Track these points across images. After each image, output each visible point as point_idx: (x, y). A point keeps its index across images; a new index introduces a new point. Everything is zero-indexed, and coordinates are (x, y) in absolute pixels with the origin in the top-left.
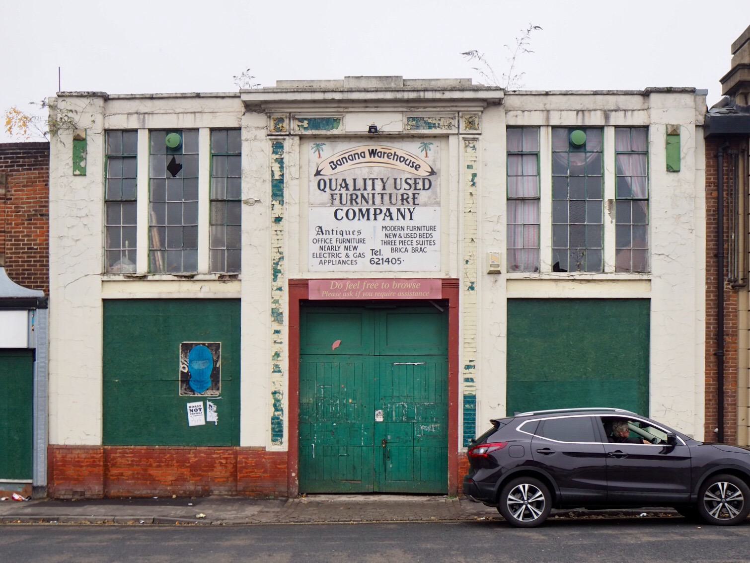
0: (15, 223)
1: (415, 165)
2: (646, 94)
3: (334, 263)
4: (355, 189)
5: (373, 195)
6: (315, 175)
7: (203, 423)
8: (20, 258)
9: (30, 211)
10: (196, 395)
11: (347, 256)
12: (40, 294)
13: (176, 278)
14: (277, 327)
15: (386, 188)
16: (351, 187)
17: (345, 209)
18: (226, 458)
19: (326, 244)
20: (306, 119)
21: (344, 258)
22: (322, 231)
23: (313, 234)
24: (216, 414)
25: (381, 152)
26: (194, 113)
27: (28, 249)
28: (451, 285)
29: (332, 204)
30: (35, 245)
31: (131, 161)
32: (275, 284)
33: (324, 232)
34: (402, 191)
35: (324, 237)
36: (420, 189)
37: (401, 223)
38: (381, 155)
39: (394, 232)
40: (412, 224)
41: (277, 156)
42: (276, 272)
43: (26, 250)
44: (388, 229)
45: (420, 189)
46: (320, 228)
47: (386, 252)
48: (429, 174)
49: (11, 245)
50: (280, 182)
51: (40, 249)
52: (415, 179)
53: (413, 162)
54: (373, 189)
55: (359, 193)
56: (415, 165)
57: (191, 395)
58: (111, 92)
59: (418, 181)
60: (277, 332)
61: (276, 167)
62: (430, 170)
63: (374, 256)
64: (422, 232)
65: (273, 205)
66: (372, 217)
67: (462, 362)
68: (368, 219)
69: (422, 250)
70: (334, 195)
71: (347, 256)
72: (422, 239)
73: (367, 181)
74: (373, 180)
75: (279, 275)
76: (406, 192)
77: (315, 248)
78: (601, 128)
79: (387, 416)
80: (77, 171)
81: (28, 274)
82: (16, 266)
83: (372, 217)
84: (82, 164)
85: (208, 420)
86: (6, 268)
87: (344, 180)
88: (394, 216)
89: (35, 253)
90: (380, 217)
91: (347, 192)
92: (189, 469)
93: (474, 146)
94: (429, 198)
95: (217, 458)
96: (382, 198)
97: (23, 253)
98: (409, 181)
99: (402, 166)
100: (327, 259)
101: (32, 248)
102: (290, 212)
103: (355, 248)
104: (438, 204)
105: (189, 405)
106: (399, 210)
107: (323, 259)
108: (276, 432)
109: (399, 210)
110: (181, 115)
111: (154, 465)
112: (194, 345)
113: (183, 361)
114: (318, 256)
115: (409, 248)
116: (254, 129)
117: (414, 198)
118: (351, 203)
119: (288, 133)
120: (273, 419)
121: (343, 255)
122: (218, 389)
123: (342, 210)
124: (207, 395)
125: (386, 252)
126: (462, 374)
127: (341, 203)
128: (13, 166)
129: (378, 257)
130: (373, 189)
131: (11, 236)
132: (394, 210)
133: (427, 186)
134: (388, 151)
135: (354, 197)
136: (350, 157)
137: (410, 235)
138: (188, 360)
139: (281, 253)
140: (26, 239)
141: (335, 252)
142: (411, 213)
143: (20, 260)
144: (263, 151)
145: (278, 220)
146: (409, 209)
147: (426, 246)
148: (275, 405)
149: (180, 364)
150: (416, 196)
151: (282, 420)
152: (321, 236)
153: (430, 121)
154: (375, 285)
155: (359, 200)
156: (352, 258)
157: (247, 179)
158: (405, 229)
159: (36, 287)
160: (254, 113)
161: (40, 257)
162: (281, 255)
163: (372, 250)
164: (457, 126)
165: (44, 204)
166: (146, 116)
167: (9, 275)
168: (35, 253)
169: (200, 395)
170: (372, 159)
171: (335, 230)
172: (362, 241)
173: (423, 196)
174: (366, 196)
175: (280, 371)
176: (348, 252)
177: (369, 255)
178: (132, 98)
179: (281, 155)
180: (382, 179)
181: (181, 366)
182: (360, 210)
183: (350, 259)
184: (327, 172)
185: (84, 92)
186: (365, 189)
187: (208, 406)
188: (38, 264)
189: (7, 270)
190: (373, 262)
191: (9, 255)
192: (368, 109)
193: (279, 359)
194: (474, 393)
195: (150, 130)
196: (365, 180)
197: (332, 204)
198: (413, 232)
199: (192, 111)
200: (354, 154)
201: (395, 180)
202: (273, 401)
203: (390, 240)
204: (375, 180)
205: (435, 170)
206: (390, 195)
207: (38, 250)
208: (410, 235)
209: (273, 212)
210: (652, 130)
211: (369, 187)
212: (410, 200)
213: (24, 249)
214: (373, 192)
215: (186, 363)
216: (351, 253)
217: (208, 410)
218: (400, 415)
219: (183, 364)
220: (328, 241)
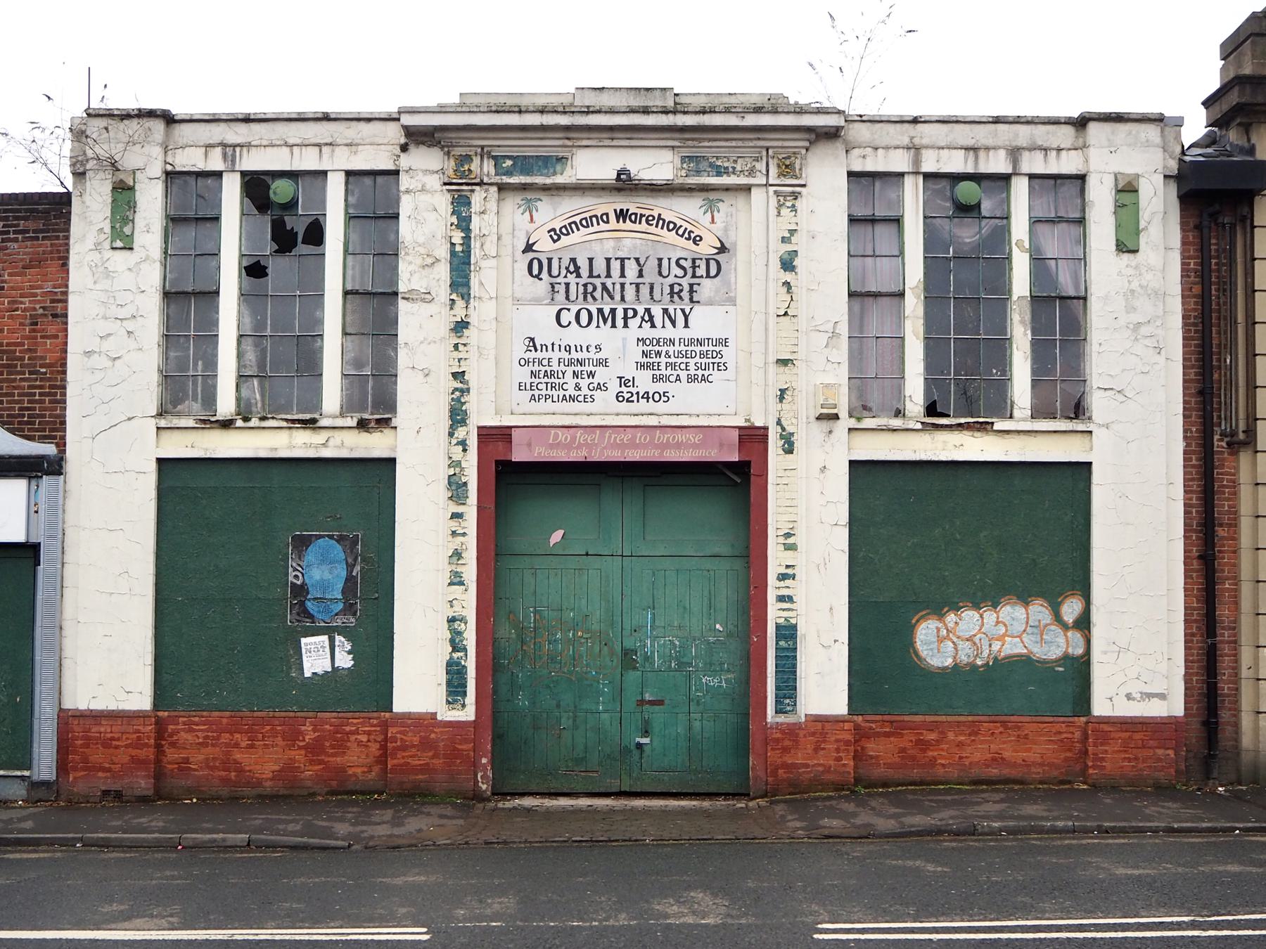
1: (693, 235)
2: (1081, 123)
3: (555, 399)
4: (591, 276)
5: (623, 285)
6: (524, 252)
8: (15, 388)
11: (578, 387)
12: (49, 449)
15: (644, 273)
16: (584, 272)
17: (574, 309)
18: (369, 733)
21: (572, 392)
23: (519, 351)
28: (753, 437)
29: (552, 299)
33: (539, 347)
34: (671, 280)
35: (539, 355)
36: (702, 277)
37: (669, 332)
38: (637, 218)
39: (657, 348)
40: (687, 334)
45: (702, 277)
46: (532, 340)
47: (644, 381)
48: (717, 251)
51: (52, 373)
52: (694, 260)
54: (623, 275)
55: (597, 282)
56: (693, 235)
58: (177, 110)
62: (719, 246)
63: (624, 389)
64: (705, 348)
66: (620, 322)
68: (614, 326)
69: (704, 379)
71: (578, 387)
73: (612, 261)
74: (622, 260)
77: (524, 375)
78: (1005, 179)
83: (620, 322)
84: (127, 230)
87: (573, 260)
88: (658, 320)
89: (41, 380)
91: (578, 280)
94: (717, 291)
96: (638, 291)
98: (682, 262)
99: (671, 237)
100: (544, 392)
101: (37, 372)
102: (481, 313)
103: (592, 375)
104: (732, 301)
105: (304, 640)
106: (665, 311)
107: (536, 393)
109: (665, 311)
111: (243, 744)
113: (294, 565)
114: (528, 387)
115: (683, 375)
116: (420, 174)
117: (691, 291)
118: (585, 298)
123: (569, 310)
125: (644, 381)
126: (773, 588)
127: (567, 298)
129: (631, 389)
130: (623, 275)
132: (657, 311)
134: (647, 213)
141: (557, 381)
143: (16, 391)
146: (683, 310)
147: (711, 371)
148: (452, 641)
149: (290, 570)
152: (532, 355)
154: (626, 437)
155: (598, 294)
156: (585, 391)
159: (43, 439)
163: (621, 378)
164: (765, 172)
165: (59, 297)
170: (621, 225)
172: (603, 363)
173: (707, 288)
174: (610, 287)
176: (579, 380)
177: (614, 387)
178: (214, 120)
180: (637, 260)
181: (291, 573)
182: (600, 311)
183: (582, 393)
186: (609, 276)
194: (793, 621)
196: (608, 260)
197: (552, 299)
198: (690, 348)
200: (591, 217)
201: (660, 260)
205: (727, 245)
209: (452, 312)
211: (616, 270)
212: (685, 295)
215: (300, 569)
216: (584, 383)
219: (295, 570)
220: (545, 362)
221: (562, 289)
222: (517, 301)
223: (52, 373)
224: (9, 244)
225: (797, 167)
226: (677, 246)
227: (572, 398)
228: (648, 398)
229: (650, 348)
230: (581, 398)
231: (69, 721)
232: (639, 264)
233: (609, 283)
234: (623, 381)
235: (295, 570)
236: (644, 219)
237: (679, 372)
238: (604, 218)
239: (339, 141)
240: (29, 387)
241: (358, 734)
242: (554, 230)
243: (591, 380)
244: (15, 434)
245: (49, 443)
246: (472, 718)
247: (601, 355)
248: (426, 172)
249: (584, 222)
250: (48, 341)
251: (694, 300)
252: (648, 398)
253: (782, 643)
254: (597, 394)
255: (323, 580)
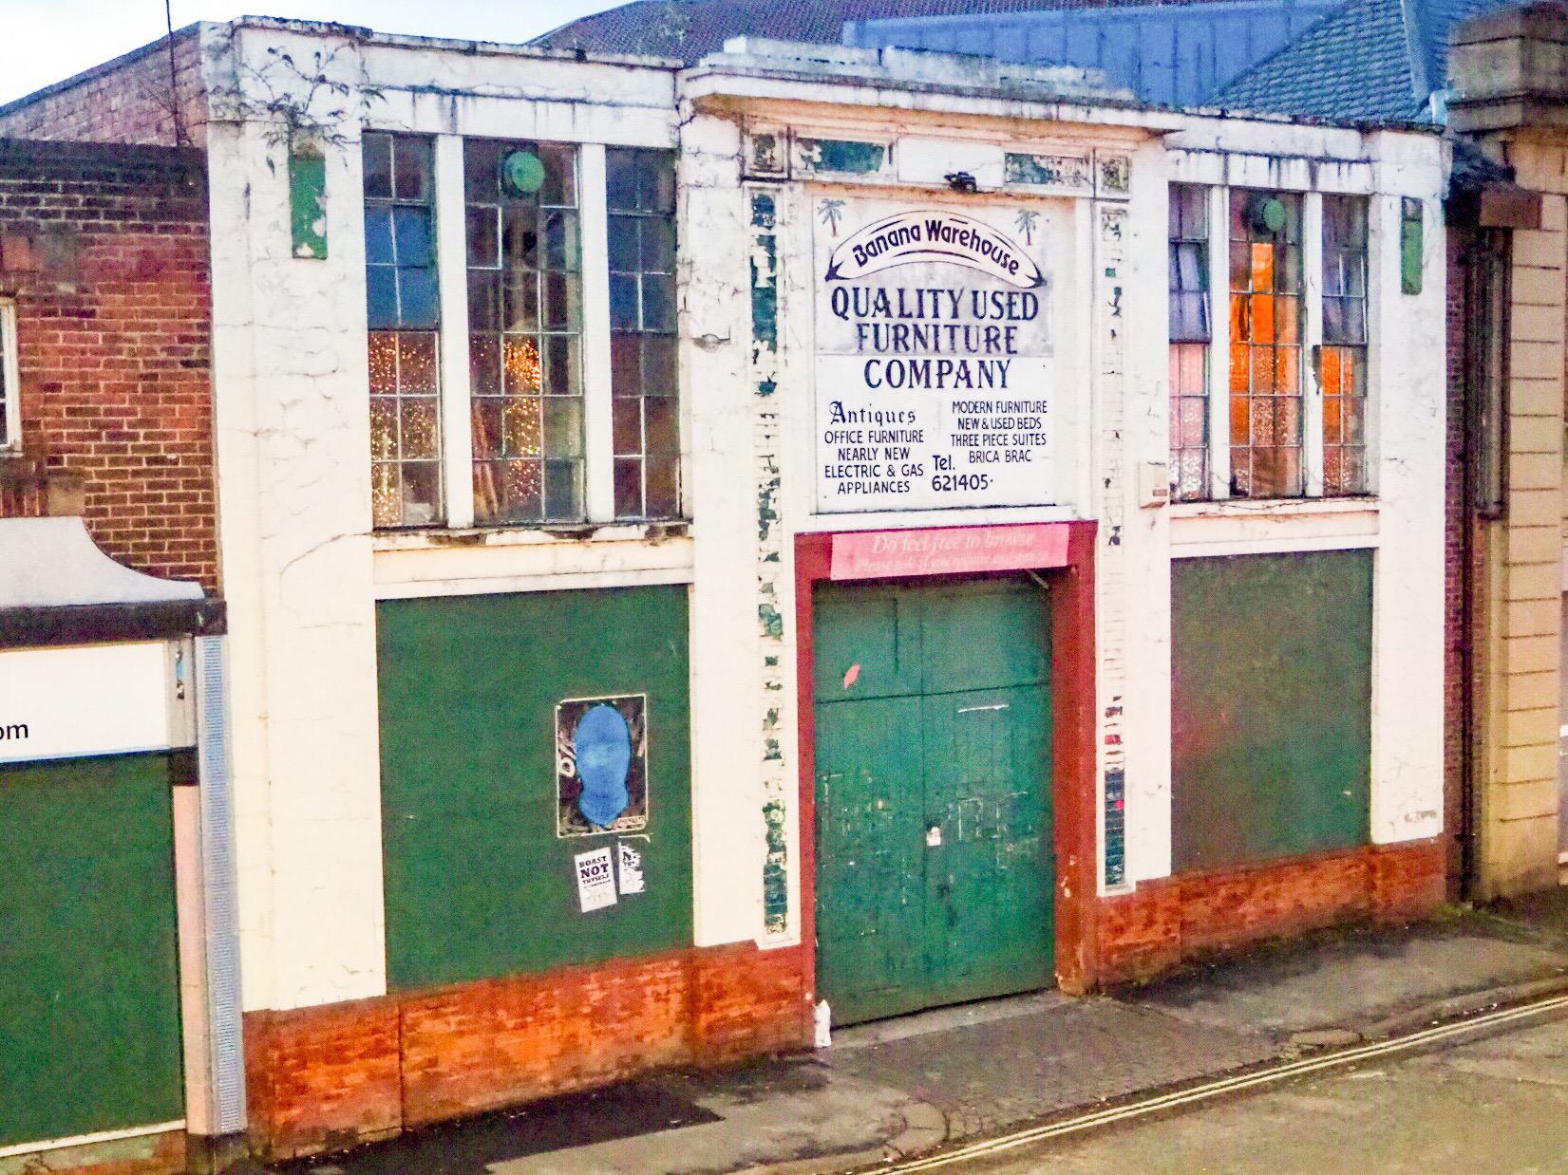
0: (107, 386)
1: (1009, 261)
3: (867, 489)
4: (902, 315)
5: (936, 327)
6: (828, 278)
7: (613, 900)
8: (126, 487)
9: (152, 352)
10: (594, 833)
12: (192, 591)
13: (552, 539)
14: (770, 647)
15: (960, 312)
16: (895, 310)
17: (885, 360)
18: (667, 981)
19: (850, 445)
20: (818, 142)
21: (884, 478)
22: (842, 414)
23: (825, 422)
24: (640, 873)
25: (949, 229)
26: (572, 101)
27: (150, 461)
28: (1083, 533)
29: (861, 347)
30: (171, 449)
31: (1176, 337)
32: (764, 545)
33: (847, 416)
34: (987, 322)
35: (848, 427)
36: (1018, 318)
39: (974, 416)
41: (763, 231)
42: (766, 516)
43: (145, 466)
44: (964, 407)
45: (1018, 318)
46: (839, 404)
47: (960, 456)
48: (1032, 283)
49: (100, 449)
50: (768, 296)
51: (187, 460)
52: (1010, 294)
53: (1007, 256)
54: (936, 315)
55: (909, 323)
56: (1009, 261)
57: (584, 835)
59: (1015, 298)
60: (771, 662)
61: (761, 257)
62: (1035, 276)
63: (941, 473)
64: (1023, 415)
65: (757, 352)
66: (934, 380)
67: (1103, 702)
68: (928, 386)
70: (865, 328)
72: (1024, 431)
73: (925, 293)
74: (935, 292)
75: (772, 523)
76: (994, 323)
77: (829, 455)
78: (1300, 196)
79: (948, 834)
80: (305, 245)
81: (153, 535)
82: (115, 512)
83: (934, 380)
84: (318, 227)
85: (623, 892)
86: (88, 520)
87: (882, 291)
89: (170, 473)
90: (949, 380)
91: (888, 320)
92: (588, 1022)
93: (1117, 227)
94: (1035, 337)
95: (647, 984)
96: (952, 337)
97: (136, 474)
98: (999, 298)
99: (985, 262)
100: (854, 480)
101: (162, 461)
102: (790, 366)
103: (905, 453)
104: (1049, 350)
105: (579, 859)
106: (982, 364)
107: (846, 480)
108: (774, 901)
109: (982, 364)
110: (540, 104)
111: (510, 1024)
112: (586, 707)
113: (564, 749)
114: (836, 473)
116: (712, 159)
117: (1008, 338)
118: (896, 348)
119: (785, 175)
120: (767, 871)
121: (882, 471)
122: (642, 812)
123: (878, 362)
124: (618, 830)
125: (962, 466)
127: (877, 346)
128: (94, 214)
129: (947, 472)
130: (936, 315)
131: (94, 424)
133: (1030, 312)
134: (961, 227)
135: (901, 332)
136: (987, 247)
137: (1002, 300)
138: (573, 745)
139: (775, 471)
140: (142, 432)
141: (867, 463)
142: (1003, 371)
143: (128, 493)
144: (732, 214)
145: (767, 388)
146: (999, 363)
147: (1029, 447)
148: (769, 838)
149: (558, 756)
150: (1012, 332)
151: (784, 872)
152: (839, 427)
153: (1043, 164)
155: (910, 340)
156: (899, 477)
157: (700, 286)
158: (994, 408)
159: (177, 574)
160: (711, 117)
161: (188, 485)
162: (775, 476)
163: (936, 457)
164: (1091, 180)
165: (196, 333)
166: (459, 99)
167: (97, 538)
168: (170, 473)
169: (602, 832)
170: (934, 245)
171: (867, 410)
172: (917, 436)
173: (1025, 332)
174: (923, 330)
175: (777, 756)
176: (892, 462)
178: (422, 44)
179: (770, 228)
180: (951, 292)
181: (559, 762)
182: (913, 363)
183: (895, 479)
184: (849, 269)
185: (320, 24)
186: (921, 315)
187: (621, 856)
188: (182, 505)
189: (89, 526)
190: (937, 486)
191: (95, 481)
192: (942, 131)
193: (777, 725)
194: (1120, 767)
195: (468, 141)
196: (920, 292)
197: (861, 347)
198: (1007, 415)
199: (565, 95)
200: (900, 231)
201: (975, 293)
202: (766, 828)
203: (968, 433)
204: (939, 294)
205: (1044, 275)
206: (967, 329)
207: (180, 466)
208: (1002, 300)
209: (757, 367)
210: (1184, 177)
211: (928, 311)
212: (1002, 342)
213: (139, 461)
214: (935, 321)
215: (569, 753)
216: (897, 465)
217: (622, 866)
218: (970, 825)
219: (564, 756)
220: (854, 437)
221: (869, 332)
222: (819, 348)
223: (187, 460)
224: (96, 236)
225: (1121, 174)
226: (992, 277)
227: (886, 488)
228: (965, 484)
229: (967, 415)
230: (894, 487)
231: (261, 1027)
232: (953, 298)
233: (921, 323)
234: (941, 462)
235: (564, 756)
236: (957, 236)
237: (997, 448)
238: (913, 233)
239: (594, 97)
240: (151, 486)
241: (656, 984)
242: (859, 248)
243: (905, 461)
244: (131, 567)
245: (188, 580)
246: (797, 941)
247: (915, 426)
248: (719, 156)
249: (893, 237)
250: (177, 407)
251: (1012, 349)
252: (965, 484)
253: (1111, 796)
254: (912, 479)
255: (601, 768)
